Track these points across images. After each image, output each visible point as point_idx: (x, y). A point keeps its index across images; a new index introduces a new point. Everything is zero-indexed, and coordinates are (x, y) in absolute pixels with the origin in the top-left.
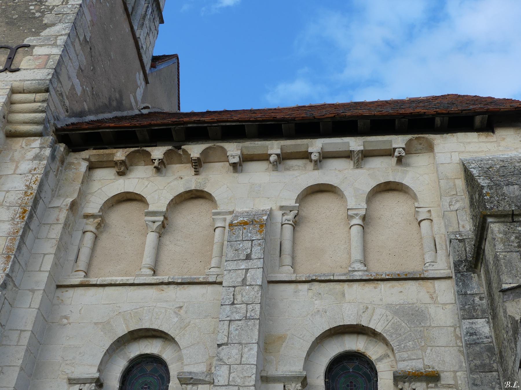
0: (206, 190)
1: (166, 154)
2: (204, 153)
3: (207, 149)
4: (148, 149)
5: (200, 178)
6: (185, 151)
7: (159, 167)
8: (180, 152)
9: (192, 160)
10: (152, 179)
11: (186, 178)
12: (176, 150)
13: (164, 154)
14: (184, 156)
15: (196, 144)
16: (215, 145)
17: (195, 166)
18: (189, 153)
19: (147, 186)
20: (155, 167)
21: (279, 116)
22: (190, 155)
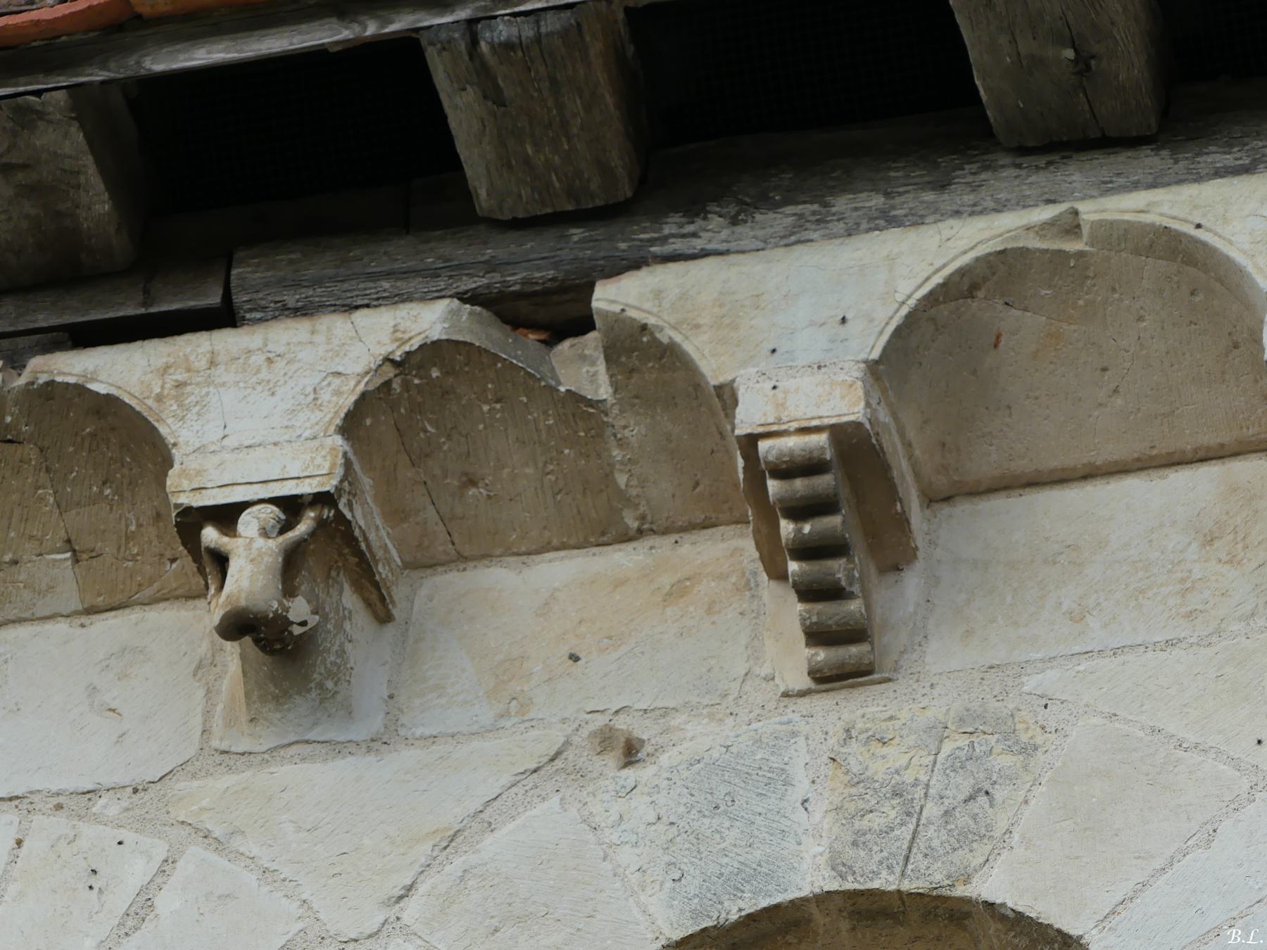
0: (995, 885)
1: (385, 415)
2: (933, 342)
3: (962, 288)
4: (116, 370)
5: (897, 722)
6: (638, 350)
7: (299, 609)
8: (581, 369)
9: (757, 471)
10: (206, 794)
11: (698, 737)
12: (520, 349)
13: (351, 425)
14: (633, 428)
15: (792, 238)
16: (1071, 227)
17: (805, 551)
18: (713, 369)
19: (141, 909)
20: (238, 625)
21: (1149, 161)
22: (727, 396)
